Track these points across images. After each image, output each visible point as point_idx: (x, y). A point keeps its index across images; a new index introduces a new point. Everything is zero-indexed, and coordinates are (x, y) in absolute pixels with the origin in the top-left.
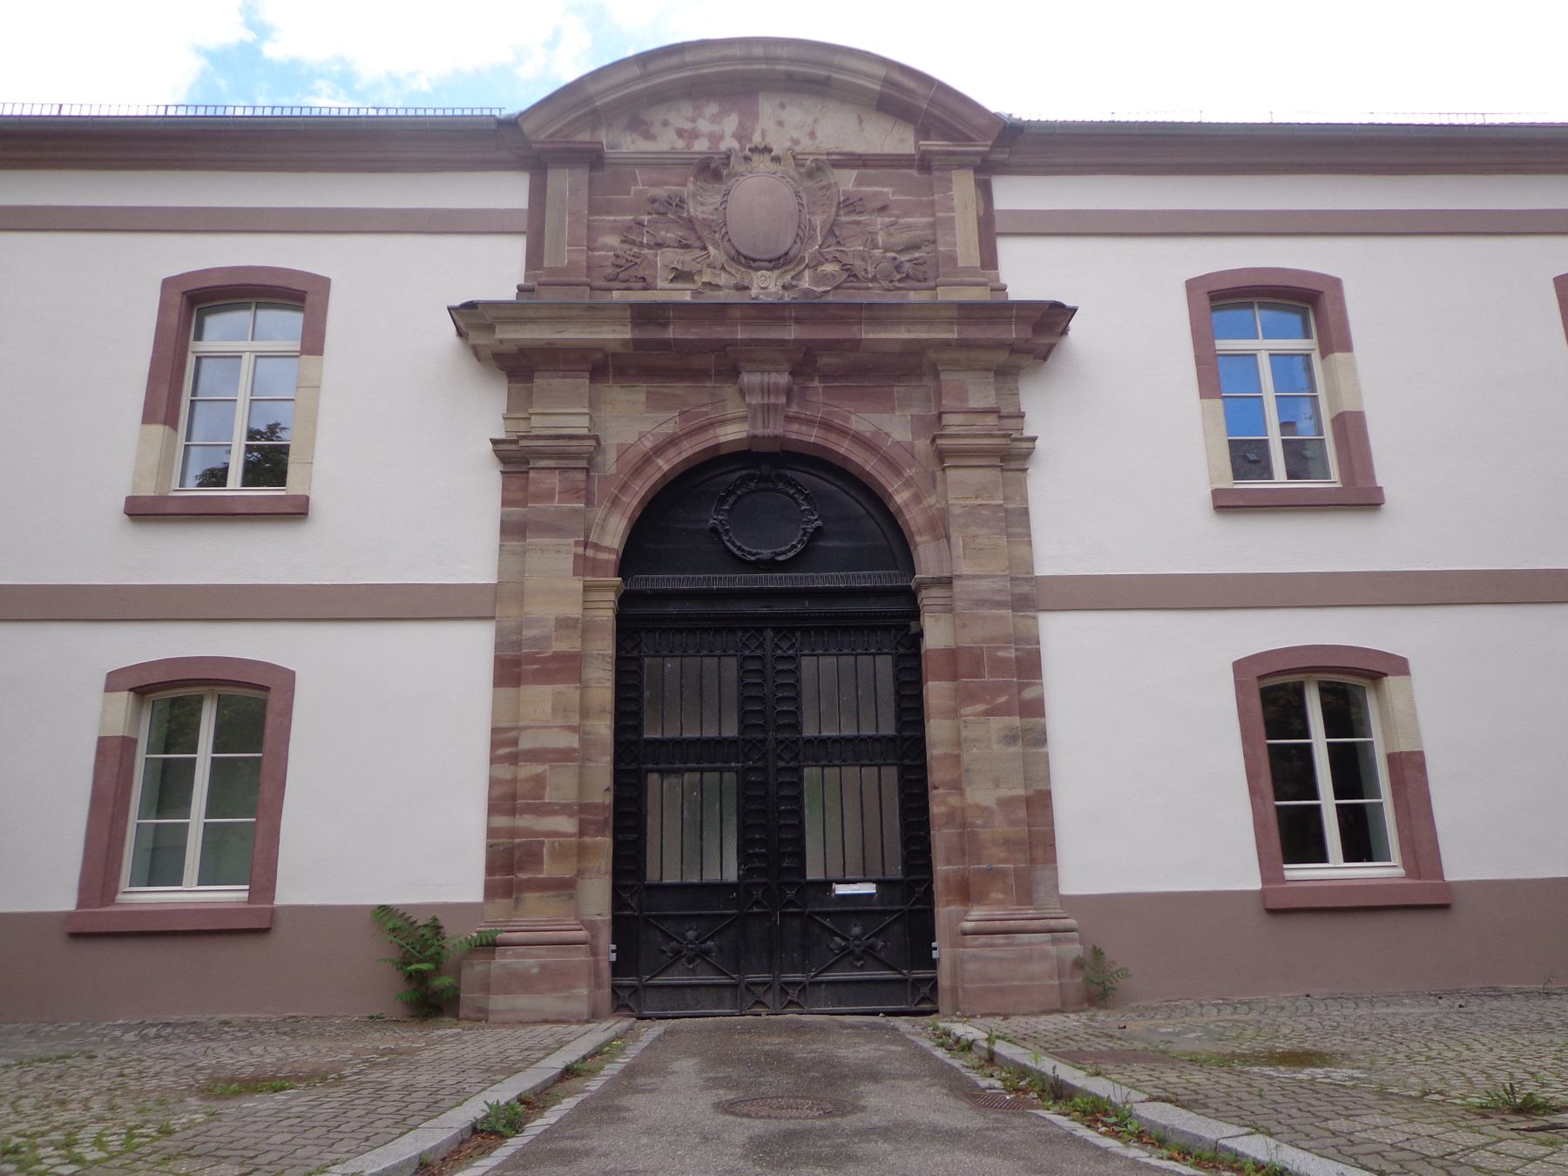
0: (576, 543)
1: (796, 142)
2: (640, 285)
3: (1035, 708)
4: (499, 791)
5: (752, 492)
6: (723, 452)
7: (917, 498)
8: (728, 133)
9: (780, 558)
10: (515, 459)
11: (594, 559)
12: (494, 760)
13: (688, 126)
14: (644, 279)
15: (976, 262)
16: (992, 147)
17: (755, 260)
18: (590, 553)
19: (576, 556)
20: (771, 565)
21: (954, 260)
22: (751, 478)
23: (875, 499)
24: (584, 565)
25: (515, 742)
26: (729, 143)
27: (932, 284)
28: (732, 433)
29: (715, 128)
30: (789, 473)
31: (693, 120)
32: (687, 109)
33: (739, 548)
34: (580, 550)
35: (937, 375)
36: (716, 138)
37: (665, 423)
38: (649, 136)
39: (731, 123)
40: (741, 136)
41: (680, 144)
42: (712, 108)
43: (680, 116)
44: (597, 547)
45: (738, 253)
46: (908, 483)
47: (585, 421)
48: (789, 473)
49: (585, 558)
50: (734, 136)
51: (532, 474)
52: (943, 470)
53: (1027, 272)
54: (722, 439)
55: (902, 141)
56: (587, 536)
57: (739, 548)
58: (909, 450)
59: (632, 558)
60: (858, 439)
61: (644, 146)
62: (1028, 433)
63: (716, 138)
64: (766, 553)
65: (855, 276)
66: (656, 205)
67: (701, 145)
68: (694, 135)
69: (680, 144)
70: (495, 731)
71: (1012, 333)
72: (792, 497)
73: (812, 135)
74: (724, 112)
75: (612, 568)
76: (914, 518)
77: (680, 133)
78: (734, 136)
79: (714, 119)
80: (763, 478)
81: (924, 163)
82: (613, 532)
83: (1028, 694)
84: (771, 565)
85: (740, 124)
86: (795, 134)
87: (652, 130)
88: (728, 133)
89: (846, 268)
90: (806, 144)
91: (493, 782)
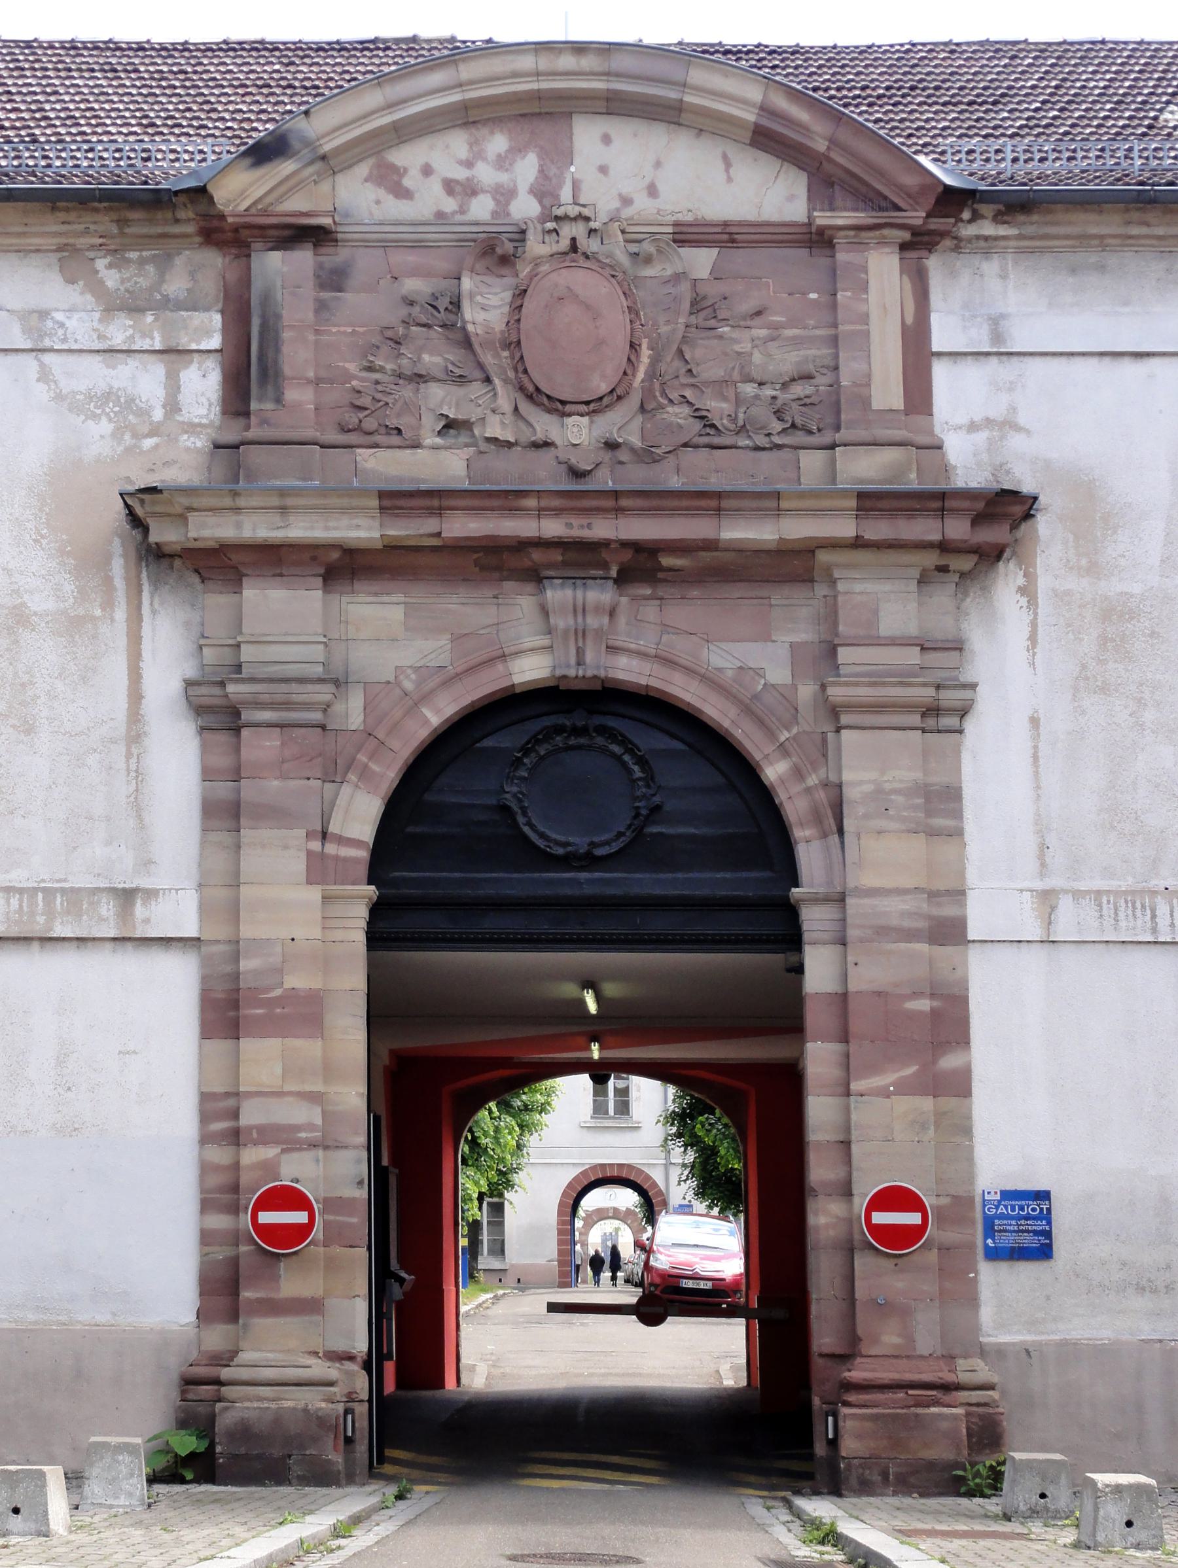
0: (309, 835)
1: (627, 201)
2: (395, 440)
3: (959, 1085)
4: (214, 1180)
5: (558, 750)
6: (518, 691)
7: (798, 773)
8: (523, 188)
9: (599, 852)
10: (219, 712)
11: (337, 858)
12: (205, 1139)
13: (460, 174)
14: (399, 431)
15: (898, 403)
16: (929, 216)
17: (563, 403)
18: (331, 849)
19: (310, 854)
20: (589, 860)
21: (866, 402)
22: (559, 730)
23: (741, 770)
24: (319, 870)
25: (235, 1114)
26: (525, 208)
27: (827, 438)
28: (530, 670)
29: (503, 178)
30: (611, 722)
31: (469, 164)
32: (458, 143)
33: (542, 835)
34: (315, 845)
35: (833, 582)
36: (503, 195)
37: (433, 650)
38: (403, 193)
39: (527, 168)
40: (544, 192)
41: (450, 205)
42: (498, 143)
43: (446, 154)
44: (341, 840)
45: (538, 389)
46: (784, 750)
47: (318, 653)
48: (611, 722)
49: (323, 856)
50: (532, 191)
51: (245, 732)
52: (838, 730)
53: (972, 427)
54: (518, 679)
55: (791, 198)
56: (325, 820)
57: (542, 835)
58: (787, 695)
59: (390, 849)
60: (710, 680)
61: (395, 209)
62: (967, 677)
63: (503, 195)
64: (580, 842)
65: (713, 426)
66: (416, 310)
67: (481, 208)
68: (470, 190)
69: (450, 205)
70: (205, 1098)
71: (958, 529)
72: (618, 758)
73: (652, 191)
74: (517, 150)
75: (363, 872)
76: (794, 806)
77: (450, 186)
78: (532, 191)
79: (502, 163)
80: (576, 731)
81: (818, 240)
82: (360, 815)
83: (949, 1062)
84: (589, 860)
85: (541, 171)
86: (626, 190)
87: (407, 182)
88: (523, 188)
89: (701, 417)
90: (643, 205)
91: (205, 1169)
